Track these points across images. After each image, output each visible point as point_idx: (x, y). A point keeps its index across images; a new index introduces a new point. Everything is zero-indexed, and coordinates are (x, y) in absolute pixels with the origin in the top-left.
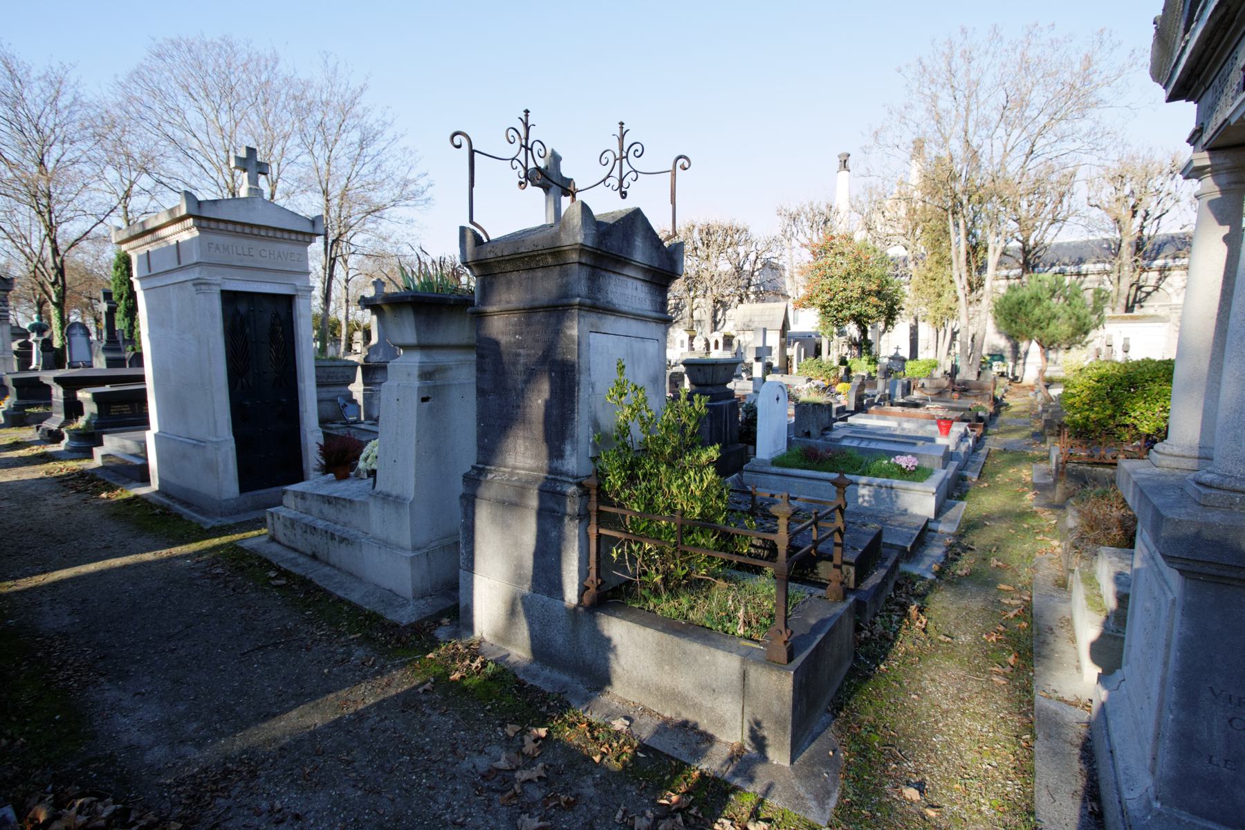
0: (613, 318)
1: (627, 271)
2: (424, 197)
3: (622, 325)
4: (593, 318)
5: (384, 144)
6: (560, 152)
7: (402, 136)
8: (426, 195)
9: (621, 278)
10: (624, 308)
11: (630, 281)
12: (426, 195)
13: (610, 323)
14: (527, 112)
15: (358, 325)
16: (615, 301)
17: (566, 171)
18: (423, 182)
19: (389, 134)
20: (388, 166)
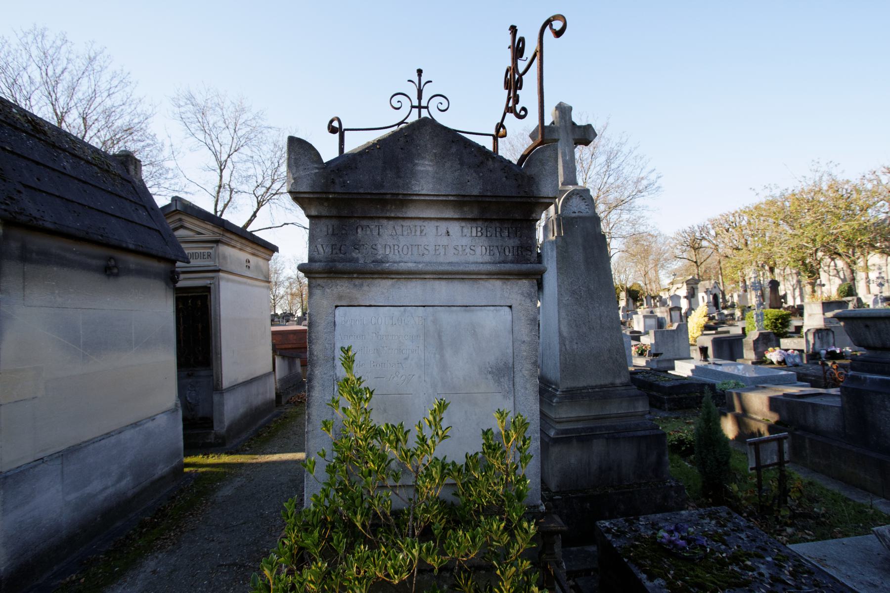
0: (419, 282)
1: (412, 212)
2: (654, 187)
3: (412, 291)
4: (343, 287)
5: (623, 158)
6: (568, 102)
7: (636, 148)
8: (657, 185)
9: (407, 223)
10: (403, 267)
11: (430, 227)
12: (657, 185)
13: (379, 290)
14: (420, 72)
15: (622, 287)
16: (393, 256)
17: (579, 119)
18: (653, 177)
19: (625, 149)
20: (627, 171)
